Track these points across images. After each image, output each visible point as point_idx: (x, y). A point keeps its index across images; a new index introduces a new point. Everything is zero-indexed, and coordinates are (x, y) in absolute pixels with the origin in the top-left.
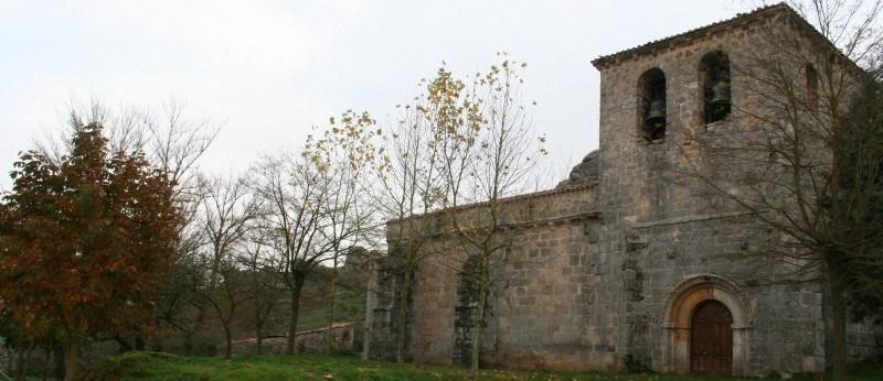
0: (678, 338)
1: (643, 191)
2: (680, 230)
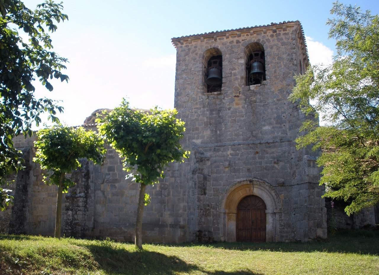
0: (229, 219)
1: (206, 124)
2: (233, 150)
